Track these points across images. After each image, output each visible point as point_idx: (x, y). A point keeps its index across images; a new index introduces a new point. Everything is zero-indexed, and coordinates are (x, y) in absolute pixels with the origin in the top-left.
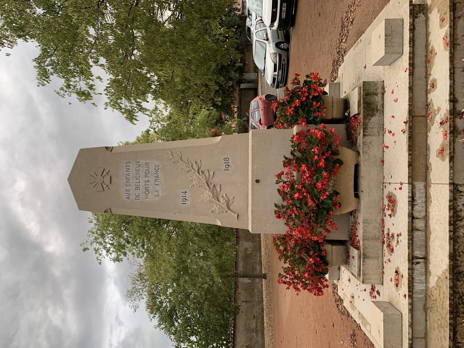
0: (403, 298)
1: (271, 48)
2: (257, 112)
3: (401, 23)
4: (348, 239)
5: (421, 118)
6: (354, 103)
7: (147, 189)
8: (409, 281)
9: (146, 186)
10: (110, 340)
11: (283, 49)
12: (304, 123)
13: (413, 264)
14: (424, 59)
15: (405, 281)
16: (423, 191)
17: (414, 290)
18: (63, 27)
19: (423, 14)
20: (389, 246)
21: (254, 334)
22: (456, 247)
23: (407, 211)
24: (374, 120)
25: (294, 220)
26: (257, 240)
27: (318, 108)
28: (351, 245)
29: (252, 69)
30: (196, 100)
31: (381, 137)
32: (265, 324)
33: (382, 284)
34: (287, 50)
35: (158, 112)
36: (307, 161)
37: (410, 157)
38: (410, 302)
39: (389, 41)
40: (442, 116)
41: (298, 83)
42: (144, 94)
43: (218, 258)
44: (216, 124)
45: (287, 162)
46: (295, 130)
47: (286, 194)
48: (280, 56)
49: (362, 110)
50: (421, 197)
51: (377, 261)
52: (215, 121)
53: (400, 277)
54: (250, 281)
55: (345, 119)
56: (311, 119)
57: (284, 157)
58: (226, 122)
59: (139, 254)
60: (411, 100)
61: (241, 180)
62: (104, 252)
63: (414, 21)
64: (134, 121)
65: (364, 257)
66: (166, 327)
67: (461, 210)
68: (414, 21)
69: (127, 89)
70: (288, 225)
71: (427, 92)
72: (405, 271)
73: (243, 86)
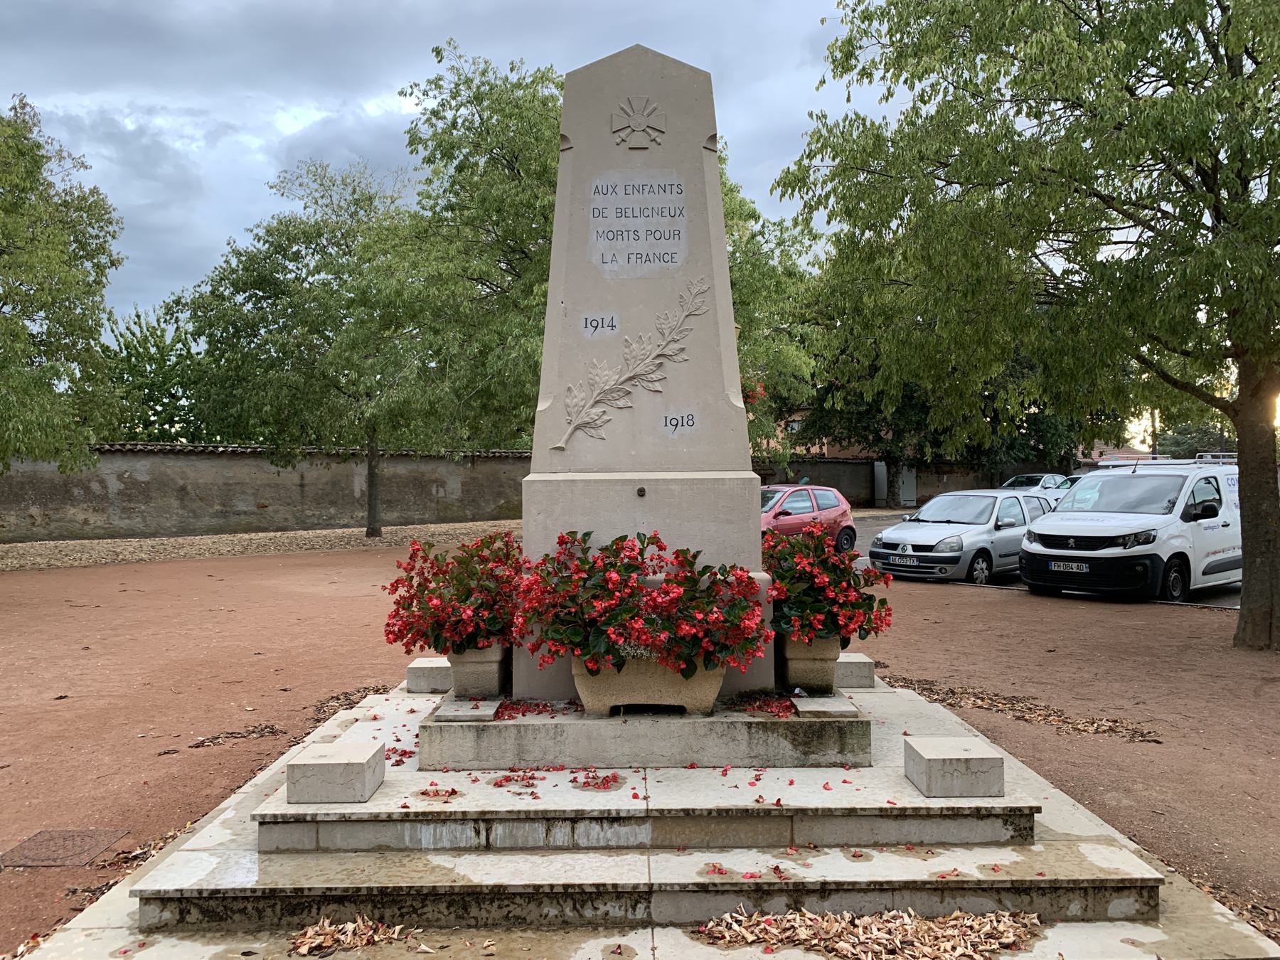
0: (401, 803)
1: (973, 537)
2: (808, 504)
3: (995, 791)
4: (514, 698)
5: (788, 834)
6: (823, 705)
7: (617, 235)
8: (439, 813)
9: (625, 234)
10: (164, 108)
11: (971, 569)
12: (775, 593)
13: (476, 821)
14: (915, 839)
15: (437, 806)
16: (632, 841)
17: (419, 825)
18: (1010, 13)
19: (1012, 837)
20: (508, 779)
21: (218, 507)
22: (518, 900)
23: (588, 808)
24: (785, 747)
25: (556, 575)
26: (468, 512)
27: (811, 625)
28: (500, 706)
29: (926, 493)
30: (836, 343)
31: (747, 761)
32: (246, 536)
33: (420, 770)
34: (970, 579)
35: (807, 242)
36: (692, 600)
37: (705, 813)
38: (395, 817)
39: (955, 766)
40: (792, 871)
41: (868, 583)
42: (849, 213)
43: (428, 407)
44: (776, 397)
45: (685, 559)
46: (761, 576)
47: (617, 553)
48: (954, 561)
49: (806, 720)
50: (619, 838)
51: (471, 757)
52: (785, 394)
53: (445, 798)
54: (357, 494)
55: (784, 688)
56: (786, 610)
57: (699, 552)
58: (782, 423)
59: (429, 197)
60: (828, 814)
61: (645, 448)
62: (432, 104)
63: (997, 816)
64: (779, 190)
65: (480, 728)
66: (233, 271)
67: (596, 909)
68: (997, 816)
69: (863, 168)
70: (544, 561)
71: (843, 846)
72: (455, 806)
73: (881, 467)
